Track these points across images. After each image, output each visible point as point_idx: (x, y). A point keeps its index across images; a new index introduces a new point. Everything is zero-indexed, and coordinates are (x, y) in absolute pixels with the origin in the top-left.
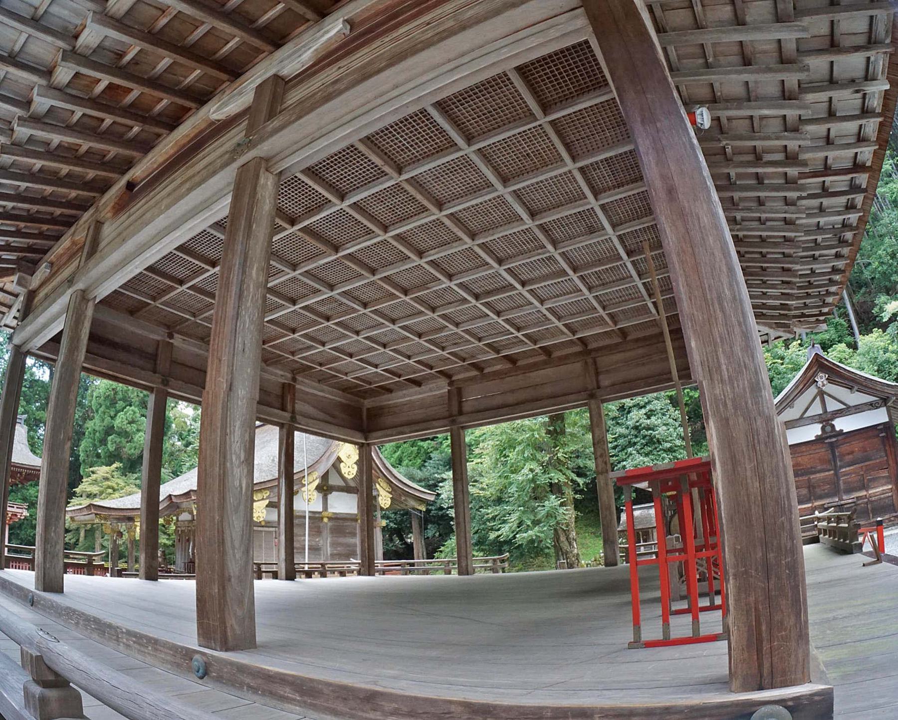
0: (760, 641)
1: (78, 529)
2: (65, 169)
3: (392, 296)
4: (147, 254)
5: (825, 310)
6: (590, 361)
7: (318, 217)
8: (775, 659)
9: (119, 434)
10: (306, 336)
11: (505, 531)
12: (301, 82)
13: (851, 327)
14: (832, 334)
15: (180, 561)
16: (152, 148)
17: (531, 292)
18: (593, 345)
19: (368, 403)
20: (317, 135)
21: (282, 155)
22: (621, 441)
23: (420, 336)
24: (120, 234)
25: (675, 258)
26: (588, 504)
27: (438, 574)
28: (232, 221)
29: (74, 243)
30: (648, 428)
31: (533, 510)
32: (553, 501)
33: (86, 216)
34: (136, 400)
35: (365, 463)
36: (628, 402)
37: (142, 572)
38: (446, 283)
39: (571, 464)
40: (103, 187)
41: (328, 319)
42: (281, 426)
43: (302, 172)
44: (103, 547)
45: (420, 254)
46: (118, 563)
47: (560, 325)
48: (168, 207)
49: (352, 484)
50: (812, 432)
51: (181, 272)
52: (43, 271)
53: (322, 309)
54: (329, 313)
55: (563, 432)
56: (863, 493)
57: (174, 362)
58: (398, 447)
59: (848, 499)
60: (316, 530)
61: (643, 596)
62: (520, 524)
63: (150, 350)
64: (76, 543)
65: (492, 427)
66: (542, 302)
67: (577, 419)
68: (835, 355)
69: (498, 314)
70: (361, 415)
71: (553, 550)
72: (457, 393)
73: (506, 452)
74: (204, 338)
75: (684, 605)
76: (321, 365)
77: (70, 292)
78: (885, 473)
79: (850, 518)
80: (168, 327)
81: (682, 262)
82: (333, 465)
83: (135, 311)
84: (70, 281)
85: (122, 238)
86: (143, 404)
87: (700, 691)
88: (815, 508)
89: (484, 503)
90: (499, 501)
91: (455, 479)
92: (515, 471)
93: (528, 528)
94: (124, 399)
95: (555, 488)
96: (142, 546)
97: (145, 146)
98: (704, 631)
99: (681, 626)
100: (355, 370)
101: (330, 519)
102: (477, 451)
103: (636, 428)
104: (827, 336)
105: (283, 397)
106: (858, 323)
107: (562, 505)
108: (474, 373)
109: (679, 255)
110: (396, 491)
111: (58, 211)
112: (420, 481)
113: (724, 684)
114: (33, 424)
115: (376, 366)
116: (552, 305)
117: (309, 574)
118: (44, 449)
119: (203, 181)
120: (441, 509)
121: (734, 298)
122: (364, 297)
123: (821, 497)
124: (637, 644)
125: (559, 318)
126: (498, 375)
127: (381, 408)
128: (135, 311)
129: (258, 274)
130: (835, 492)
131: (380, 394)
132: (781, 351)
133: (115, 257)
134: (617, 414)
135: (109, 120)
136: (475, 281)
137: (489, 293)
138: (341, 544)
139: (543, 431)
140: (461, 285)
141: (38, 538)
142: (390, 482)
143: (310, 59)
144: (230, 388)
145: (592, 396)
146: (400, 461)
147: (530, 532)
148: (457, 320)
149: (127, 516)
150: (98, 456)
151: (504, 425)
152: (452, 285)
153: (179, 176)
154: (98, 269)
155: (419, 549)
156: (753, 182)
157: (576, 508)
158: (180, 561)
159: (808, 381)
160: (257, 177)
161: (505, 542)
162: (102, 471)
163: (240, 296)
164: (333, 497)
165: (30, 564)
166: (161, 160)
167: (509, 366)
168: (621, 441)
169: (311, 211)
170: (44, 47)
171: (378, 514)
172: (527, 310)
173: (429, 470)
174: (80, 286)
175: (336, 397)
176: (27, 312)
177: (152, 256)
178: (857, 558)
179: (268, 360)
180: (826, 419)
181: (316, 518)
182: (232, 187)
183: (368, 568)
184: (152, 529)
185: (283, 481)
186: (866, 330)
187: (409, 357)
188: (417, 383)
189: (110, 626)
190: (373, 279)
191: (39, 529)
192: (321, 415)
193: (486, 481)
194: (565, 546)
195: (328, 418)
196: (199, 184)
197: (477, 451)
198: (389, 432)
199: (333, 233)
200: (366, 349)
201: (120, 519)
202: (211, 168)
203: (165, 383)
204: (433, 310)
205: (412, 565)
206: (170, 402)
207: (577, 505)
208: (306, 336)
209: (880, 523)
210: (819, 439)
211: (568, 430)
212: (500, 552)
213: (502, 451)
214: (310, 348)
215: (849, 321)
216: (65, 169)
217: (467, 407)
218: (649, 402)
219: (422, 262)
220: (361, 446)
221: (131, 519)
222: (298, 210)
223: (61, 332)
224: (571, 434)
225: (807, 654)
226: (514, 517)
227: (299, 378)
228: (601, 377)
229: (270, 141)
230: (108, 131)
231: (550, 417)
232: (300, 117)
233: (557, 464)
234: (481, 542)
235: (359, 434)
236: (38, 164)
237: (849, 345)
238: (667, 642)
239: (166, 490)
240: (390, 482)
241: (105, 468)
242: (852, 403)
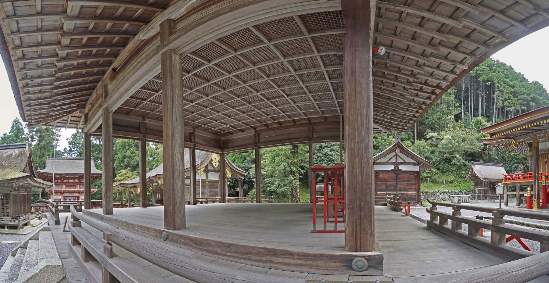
0: (356, 234)
1: (116, 193)
2: (84, 71)
3: (233, 98)
4: (130, 91)
5: (406, 128)
6: (311, 127)
7: (199, 70)
8: (362, 241)
9: (128, 158)
10: (198, 114)
11: (273, 188)
12: (183, 20)
13: (414, 136)
14: (407, 137)
15: (153, 200)
17: (291, 99)
18: (312, 121)
19: (223, 138)
20: (196, 38)
21: (181, 48)
22: (319, 159)
23: (244, 113)
24: (116, 87)
25: (347, 97)
26: (304, 180)
28: (164, 74)
29: (98, 95)
30: (330, 155)
31: (284, 180)
32: (291, 177)
33: (99, 84)
34: (133, 145)
35: (222, 162)
36: (323, 144)
37: (141, 204)
38: (256, 93)
39: (299, 165)
40: (103, 73)
41: (206, 107)
42: (190, 148)
43: (190, 53)
44: (125, 198)
45: (245, 82)
46: (132, 203)
47: (301, 112)
48: (134, 73)
49: (217, 169)
50: (392, 167)
51: (144, 97)
52: (88, 107)
53: (204, 104)
54: (207, 105)
55: (297, 152)
56: (405, 192)
57: (146, 129)
58: (234, 155)
59: (399, 193)
60: (204, 187)
61: (318, 215)
62: (279, 185)
63: (137, 126)
64: (116, 198)
65: (270, 148)
66: (295, 103)
67: (303, 148)
68: (404, 144)
69: (276, 106)
70: (221, 143)
72: (258, 135)
73: (275, 158)
74: (159, 119)
75: (333, 219)
76: (204, 125)
77: (101, 110)
78: (414, 188)
79: (398, 199)
80: (143, 117)
81: (350, 98)
82: (210, 162)
83: (128, 113)
84: (100, 106)
85: (117, 88)
86: (136, 146)
87: (334, 250)
88: (387, 194)
89: (267, 177)
90: (271, 176)
91: (256, 167)
92: (278, 166)
93: (282, 187)
94: (128, 145)
95: (292, 173)
96: (141, 195)
98: (339, 229)
99: (330, 226)
100: (218, 126)
101: (208, 182)
102: (264, 157)
103: (325, 154)
104: (404, 137)
105: (190, 138)
106: (417, 136)
107: (295, 179)
108: (265, 128)
109: (349, 95)
110: (233, 171)
111: (87, 86)
112: (242, 168)
113: (343, 248)
114: (96, 160)
115: (226, 125)
116: (299, 103)
117: (201, 202)
118: (103, 166)
119: (147, 61)
120: (250, 178)
121: (367, 115)
122: (221, 99)
123: (390, 191)
124: (314, 231)
125: (301, 110)
126: (274, 129)
127: (228, 140)
128: (128, 113)
129: (178, 92)
130: (395, 190)
131: (228, 135)
132: (385, 137)
133: (116, 96)
134: (318, 148)
136: (268, 93)
137: (273, 98)
138: (213, 191)
139: (289, 152)
140: (262, 95)
141: (103, 197)
142: (231, 168)
143: (184, 11)
144: (173, 134)
145: (309, 140)
146: (234, 160)
147: (282, 189)
148: (260, 107)
149: (134, 186)
150: (121, 166)
151: (275, 148)
152: (258, 94)
154: (110, 101)
155: (241, 193)
156: (382, 75)
157: (300, 181)
158: (153, 200)
159: (393, 150)
160: (171, 57)
161: (273, 192)
162: (123, 171)
163: (173, 100)
164: (210, 174)
165: (101, 206)
167: (279, 126)
168: (319, 159)
169: (195, 68)
171: (226, 180)
172: (288, 105)
173: (245, 164)
174: (105, 106)
175: (210, 136)
176: (86, 121)
177: (131, 92)
178: (399, 213)
179: (186, 124)
180: (396, 164)
181: (203, 181)
182: (160, 62)
184: (144, 189)
185: (192, 168)
186: (419, 138)
187: (239, 121)
188: (242, 131)
189: (131, 224)
190: (224, 92)
191: (104, 193)
192: (205, 143)
193: (267, 168)
195: (208, 144)
196: (145, 63)
197: (264, 157)
198: (231, 149)
199: (207, 75)
200: (221, 119)
201: (131, 187)
202: (149, 57)
203: (145, 136)
204: (250, 103)
205: (238, 199)
206: (147, 142)
207: (300, 180)
208: (198, 114)
209: (409, 203)
210: (392, 171)
211: (299, 152)
212: (271, 195)
213: (273, 158)
214: (200, 118)
215: (414, 134)
216: (84, 71)
217: (261, 140)
218: (332, 146)
219: (246, 85)
220: (221, 154)
221: (135, 187)
222: (190, 68)
223: (101, 125)
224: (300, 154)
225: (373, 241)
226: (277, 182)
227: (196, 130)
228: (314, 134)
229: (174, 43)
231: (293, 146)
232: (186, 33)
233: (294, 164)
234: (264, 191)
235: (220, 150)
236: (72, 73)
237: (411, 142)
238: (325, 231)
239: (149, 174)
240: (231, 168)
241: (124, 170)
242: (407, 161)
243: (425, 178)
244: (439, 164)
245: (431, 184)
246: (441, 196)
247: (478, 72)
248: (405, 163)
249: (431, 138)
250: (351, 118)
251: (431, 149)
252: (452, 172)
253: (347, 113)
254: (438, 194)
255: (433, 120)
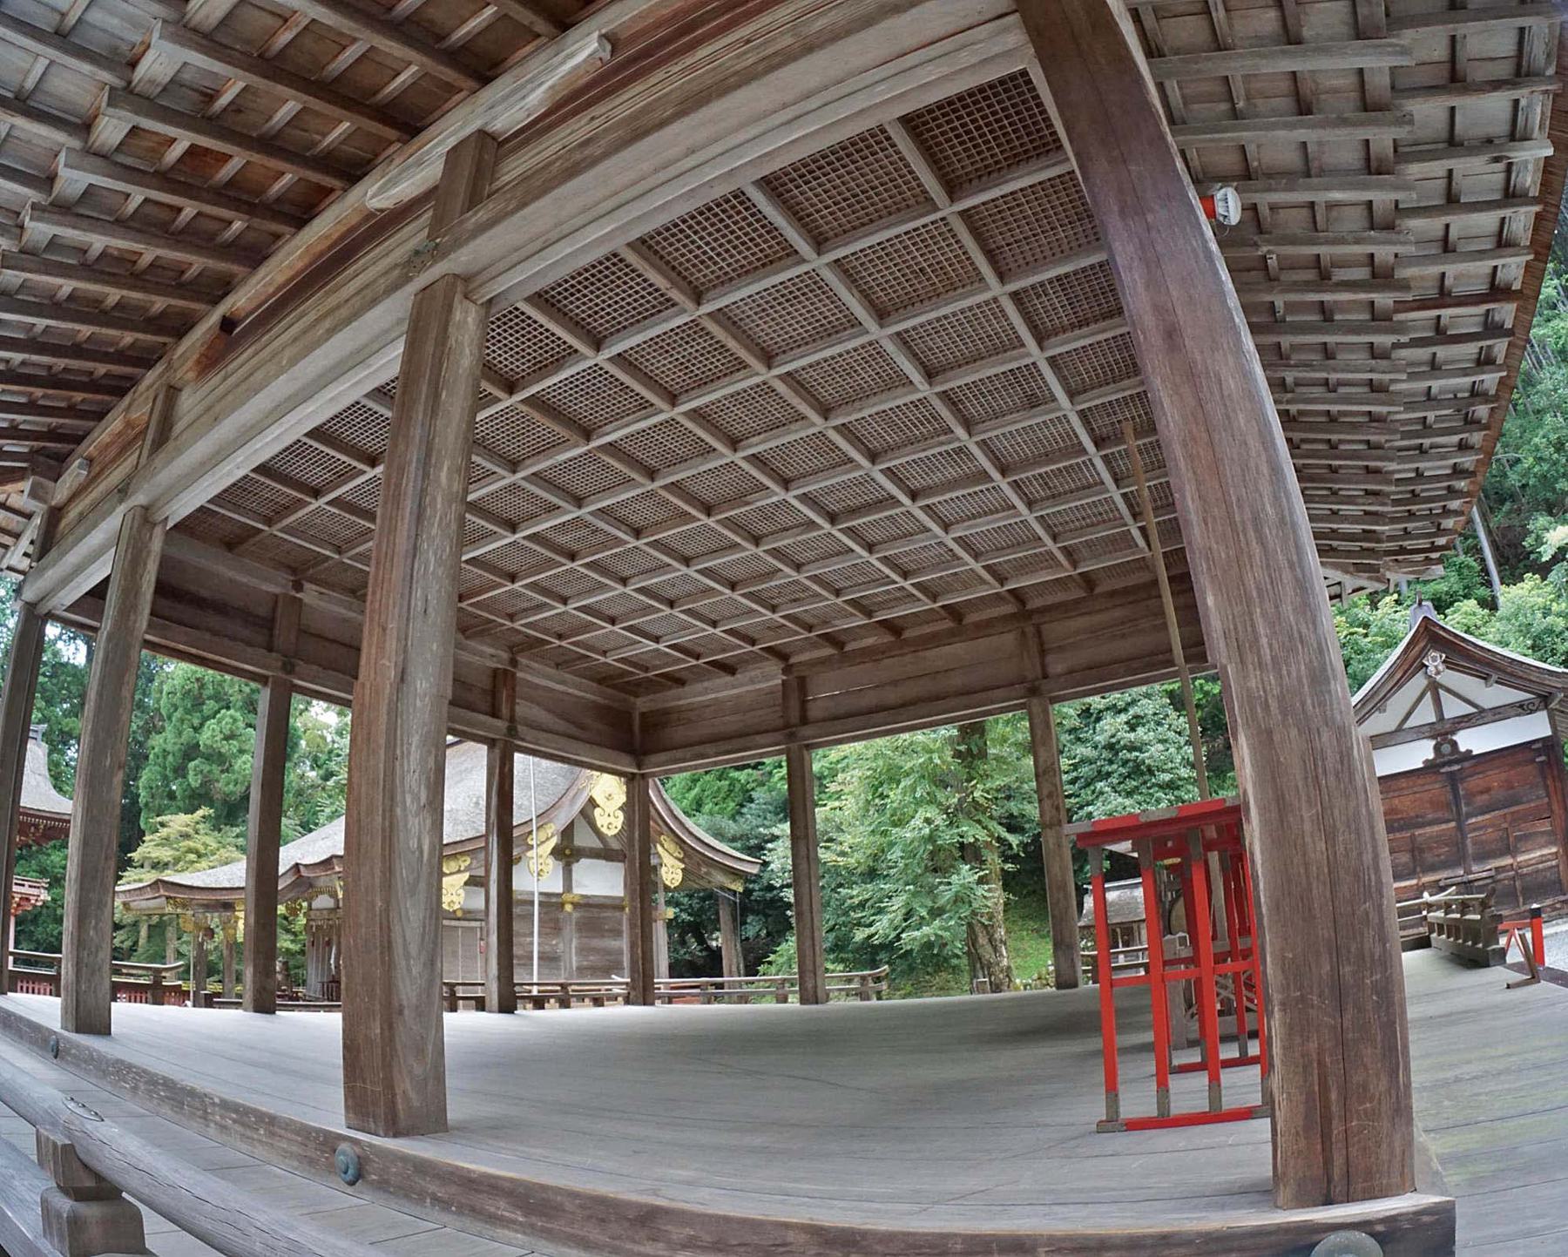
1: (135, 924)
2: (113, 295)
3: (685, 517)
4: (257, 444)
6: (1030, 630)
7: (555, 379)
8: (1354, 1151)
9: (208, 758)
10: (534, 586)
11: (882, 927)
12: (526, 142)
13: (1485, 570)
14: (1453, 583)
15: (314, 979)
16: (266, 258)
18: (1035, 603)
19: (642, 704)
20: (554, 235)
21: (493, 271)
22: (1084, 770)
23: (733, 586)
24: (209, 409)
26: (1027, 880)
27: (764, 1003)
28: (405, 386)
29: (129, 424)
30: (1132, 748)
31: (931, 891)
32: (965, 874)
33: (151, 376)
34: (237, 699)
35: (638, 809)
36: (1096, 702)
37: (248, 998)
38: (779, 494)
39: (997, 811)
40: (179, 326)
41: (572, 557)
42: (491, 743)
43: (528, 300)
44: (180, 955)
45: (734, 443)
46: (206, 983)
47: (977, 567)
48: (294, 362)
49: (615, 845)
50: (1418, 754)
51: (315, 476)
53: (562, 539)
54: (575, 547)
55: (983, 755)
56: (1508, 861)
57: (303, 632)
58: (695, 781)
59: (1480, 871)
60: (552, 925)
61: (1123, 1040)
62: (908, 915)
63: (263, 611)
64: (133, 948)
65: (859, 746)
67: (1007, 732)
68: (1458, 619)
69: (870, 548)
70: (630, 724)
71: (965, 961)
72: (798, 685)
73: (884, 789)
74: (357, 591)
75: (1195, 1057)
76: (560, 637)
77: (121, 509)
78: (1545, 826)
79: (1484, 905)
80: (294, 571)
81: (1191, 458)
82: (582, 812)
83: (235, 542)
84: (123, 491)
85: (212, 415)
86: (250, 706)
87: (1223, 1207)
88: (1423, 888)
89: (845, 877)
90: (872, 874)
91: (794, 837)
92: (899, 823)
93: (922, 922)
94: (216, 697)
95: (969, 852)
96: (248, 954)
97: (254, 254)
98: (1229, 1102)
99: (1189, 1093)
100: (620, 646)
101: (576, 905)
102: (833, 787)
103: (1110, 747)
104: (1443, 587)
105: (493, 693)
106: (1499, 564)
107: (981, 881)
108: (828, 651)
109: (1185, 445)
110: (692, 858)
111: (101, 369)
112: (733, 839)
113: (1264, 1193)
115: (657, 639)
116: (964, 532)
117: (539, 1003)
119: (355, 316)
120: (771, 888)
121: (1282, 521)
122: (636, 519)
123: (1433, 868)
124: (1113, 1124)
125: (976, 556)
126: (869, 654)
127: (666, 712)
128: (235, 542)
129: (450, 479)
130: (1458, 859)
131: (663, 688)
132: (1363, 612)
133: (200, 449)
134: (1077, 723)
135: (190, 210)
136: (830, 491)
137: (854, 512)
138: (595, 950)
139: (949, 753)
140: (805, 498)
141: (66, 940)
142: (680, 842)
143: (541, 103)
144: (402, 677)
145: (1034, 691)
146: (698, 805)
147: (925, 929)
148: (799, 558)
149: (221, 902)
150: (172, 796)
151: (880, 741)
152: (790, 497)
153: (313, 308)
154: (171, 469)
155: (731, 958)
156: (1315, 317)
157: (1006, 887)
158: (314, 979)
159: (1410, 665)
160: (449, 309)
161: (882, 947)
162: (178, 822)
163: (420, 517)
164: (582, 868)
165: (53, 985)
166: (281, 279)
167: (888, 638)
168: (1084, 770)
169: (543, 369)
170: (77, 82)
171: (661, 897)
172: (921, 541)
173: (749, 821)
174: (140, 498)
177: (266, 447)
178: (1496, 975)
179: (468, 628)
180: (1442, 732)
181: (552, 904)
182: (405, 327)
183: (642, 992)
184: (265, 924)
185: (494, 840)
186: (1512, 576)
187: (714, 624)
188: (728, 668)
189: (192, 1093)
190: (651, 486)
191: (68, 924)
192: (561, 725)
193: (848, 839)
194: (987, 953)
195: (573, 730)
196: (348, 321)
197: (833, 787)
198: (679, 754)
199: (581, 408)
200: (639, 610)
201: (210, 907)
202: (369, 294)
203: (289, 668)
204: (757, 541)
205: (720, 986)
206: (298, 702)
207: (1008, 882)
208: (534, 586)
209: (1536, 914)
210: (1430, 767)
211: (992, 751)
212: (874, 964)
213: (876, 788)
214: (540, 607)
215: (1483, 560)
216: (113, 295)
217: (815, 711)
218: (1134, 702)
219: (737, 457)
220: (630, 779)
221: (228, 906)
222: (520, 367)
223: (107, 579)
224: (998, 758)
225: (1409, 1142)
226: (898, 903)
227: (523, 660)
228: (1049, 658)
229: (472, 245)
230: (189, 229)
231: (961, 729)
232: (523, 205)
233: (972, 810)
234: (839, 947)
235: (627, 758)
236: (66, 286)
237: (1483, 603)
238: (1164, 1121)
239: (290, 855)
240: (680, 842)
241: (183, 818)
242: (1487, 704)
250: (1221, 552)
253: (1196, 531)
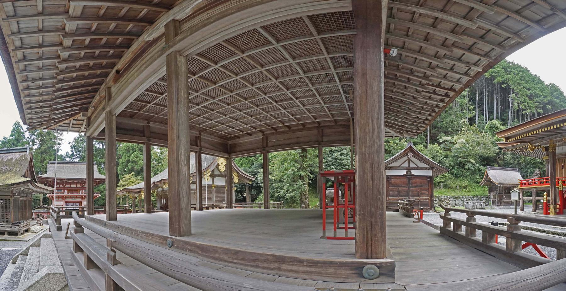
1: (120, 198)
3: (240, 101)
4: (134, 94)
6: (320, 130)
7: (206, 72)
8: (373, 248)
9: (132, 162)
10: (204, 117)
11: (282, 193)
12: (188, 20)
13: (427, 140)
14: (419, 140)
15: (158, 206)
16: (122, 56)
18: (322, 125)
19: (230, 142)
20: (202, 39)
21: (186, 49)
22: (329, 163)
23: (251, 116)
24: (119, 89)
26: (314, 185)
27: (255, 208)
28: (169, 76)
30: (340, 160)
31: (293, 185)
32: (300, 182)
33: (103, 86)
34: (137, 149)
35: (229, 166)
36: (333, 148)
37: (145, 210)
38: (264, 96)
39: (309, 169)
40: (106, 75)
41: (213, 110)
42: (196, 152)
43: (196, 55)
44: (129, 203)
45: (252, 85)
46: (136, 208)
47: (310, 115)
48: (138, 76)
49: (223, 174)
50: (404, 172)
51: (148, 99)
53: (210, 107)
54: (213, 108)
55: (306, 157)
56: (418, 198)
57: (151, 132)
58: (241, 160)
59: (412, 198)
60: (210, 192)
61: (327, 221)
62: (287, 191)
63: (141, 129)
64: (119, 203)
65: (278, 153)
67: (312, 152)
68: (416, 148)
69: (285, 109)
70: (228, 147)
71: (299, 201)
72: (266, 138)
73: (284, 163)
74: (164, 122)
75: (343, 226)
76: (211, 128)
77: (104, 113)
79: (411, 205)
80: (147, 120)
81: (360, 101)
82: (216, 167)
83: (132, 116)
84: (104, 109)
85: (121, 91)
86: (141, 150)
87: (344, 257)
88: (399, 199)
89: (275, 182)
90: (280, 181)
91: (264, 172)
92: (286, 170)
93: (291, 192)
94: (132, 150)
95: (302, 178)
96: (145, 201)
97: (119, 57)
98: (349, 236)
99: (341, 233)
100: (225, 130)
101: (215, 187)
102: (272, 162)
103: (335, 159)
104: (417, 141)
105: (196, 141)
106: (430, 140)
107: (304, 184)
108: (273, 131)
109: (360, 98)
110: (240, 176)
112: (249, 173)
113: (354, 255)
115: (233, 128)
116: (308, 106)
117: (208, 208)
119: (151, 63)
120: (257, 183)
121: (378, 118)
122: (228, 102)
123: (402, 196)
124: (323, 237)
125: (310, 113)
126: (283, 133)
127: (235, 144)
128: (132, 116)
129: (184, 94)
130: (407, 195)
131: (235, 139)
132: (397, 141)
133: (119, 99)
134: (328, 152)
135: (97, 52)
136: (276, 96)
137: (282, 101)
138: (219, 197)
139: (298, 156)
140: (270, 97)
142: (238, 173)
143: (190, 12)
144: (178, 138)
145: (319, 144)
146: (242, 165)
147: (291, 194)
148: (268, 110)
149: (139, 191)
150: (125, 171)
151: (283, 152)
152: (266, 97)
153: (138, 64)
154: (113, 104)
155: (248, 199)
156: (394, 77)
157: (309, 186)
158: (158, 206)
159: (405, 154)
160: (176, 58)
161: (281, 197)
162: (127, 176)
163: (178, 103)
164: (216, 179)
165: (104, 212)
166: (128, 60)
167: (287, 129)
168: (329, 163)
169: (202, 70)
170: (51, 37)
171: (233, 185)
172: (297, 108)
173: (253, 169)
174: (108, 109)
177: (135, 95)
178: (412, 219)
179: (192, 128)
180: (409, 169)
181: (210, 187)
182: (165, 63)
183: (230, 206)
184: (149, 195)
185: (198, 173)
186: (432, 142)
187: (247, 125)
188: (250, 134)
189: (135, 230)
190: (231, 94)
192: (211, 147)
193: (275, 173)
194: (304, 200)
195: (214, 148)
196: (150, 65)
197: (272, 162)
198: (238, 153)
199: (213, 78)
201: (135, 193)
202: (153, 58)
203: (149, 140)
204: (257, 106)
205: (246, 204)
206: (152, 146)
207: (310, 185)
208: (204, 117)
209: (422, 209)
210: (405, 176)
211: (308, 156)
212: (279, 201)
213: (282, 162)
214: (206, 122)
215: (427, 138)
217: (269, 144)
218: (342, 150)
219: (253, 88)
220: (228, 159)
221: (140, 192)
222: (196, 70)
224: (309, 158)
225: (385, 248)
226: (285, 188)
227: (202, 134)
228: (324, 137)
229: (179, 44)
230: (99, 55)
231: (302, 151)
232: (192, 34)
233: (303, 169)
234: (272, 197)
235: (226, 154)
237: (424, 146)
238: (335, 238)
239: (154, 179)
240: (238, 173)
241: (128, 175)
243: (438, 183)
244: (453, 168)
245: (445, 190)
246: (454, 202)
247: (493, 74)
248: (417, 168)
249: (444, 142)
251: (444, 153)
252: (466, 177)
254: (452, 199)
255: (447, 123)
